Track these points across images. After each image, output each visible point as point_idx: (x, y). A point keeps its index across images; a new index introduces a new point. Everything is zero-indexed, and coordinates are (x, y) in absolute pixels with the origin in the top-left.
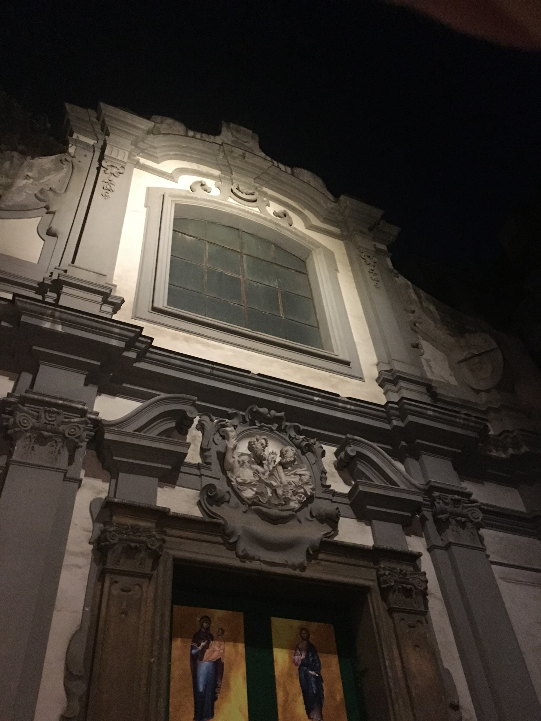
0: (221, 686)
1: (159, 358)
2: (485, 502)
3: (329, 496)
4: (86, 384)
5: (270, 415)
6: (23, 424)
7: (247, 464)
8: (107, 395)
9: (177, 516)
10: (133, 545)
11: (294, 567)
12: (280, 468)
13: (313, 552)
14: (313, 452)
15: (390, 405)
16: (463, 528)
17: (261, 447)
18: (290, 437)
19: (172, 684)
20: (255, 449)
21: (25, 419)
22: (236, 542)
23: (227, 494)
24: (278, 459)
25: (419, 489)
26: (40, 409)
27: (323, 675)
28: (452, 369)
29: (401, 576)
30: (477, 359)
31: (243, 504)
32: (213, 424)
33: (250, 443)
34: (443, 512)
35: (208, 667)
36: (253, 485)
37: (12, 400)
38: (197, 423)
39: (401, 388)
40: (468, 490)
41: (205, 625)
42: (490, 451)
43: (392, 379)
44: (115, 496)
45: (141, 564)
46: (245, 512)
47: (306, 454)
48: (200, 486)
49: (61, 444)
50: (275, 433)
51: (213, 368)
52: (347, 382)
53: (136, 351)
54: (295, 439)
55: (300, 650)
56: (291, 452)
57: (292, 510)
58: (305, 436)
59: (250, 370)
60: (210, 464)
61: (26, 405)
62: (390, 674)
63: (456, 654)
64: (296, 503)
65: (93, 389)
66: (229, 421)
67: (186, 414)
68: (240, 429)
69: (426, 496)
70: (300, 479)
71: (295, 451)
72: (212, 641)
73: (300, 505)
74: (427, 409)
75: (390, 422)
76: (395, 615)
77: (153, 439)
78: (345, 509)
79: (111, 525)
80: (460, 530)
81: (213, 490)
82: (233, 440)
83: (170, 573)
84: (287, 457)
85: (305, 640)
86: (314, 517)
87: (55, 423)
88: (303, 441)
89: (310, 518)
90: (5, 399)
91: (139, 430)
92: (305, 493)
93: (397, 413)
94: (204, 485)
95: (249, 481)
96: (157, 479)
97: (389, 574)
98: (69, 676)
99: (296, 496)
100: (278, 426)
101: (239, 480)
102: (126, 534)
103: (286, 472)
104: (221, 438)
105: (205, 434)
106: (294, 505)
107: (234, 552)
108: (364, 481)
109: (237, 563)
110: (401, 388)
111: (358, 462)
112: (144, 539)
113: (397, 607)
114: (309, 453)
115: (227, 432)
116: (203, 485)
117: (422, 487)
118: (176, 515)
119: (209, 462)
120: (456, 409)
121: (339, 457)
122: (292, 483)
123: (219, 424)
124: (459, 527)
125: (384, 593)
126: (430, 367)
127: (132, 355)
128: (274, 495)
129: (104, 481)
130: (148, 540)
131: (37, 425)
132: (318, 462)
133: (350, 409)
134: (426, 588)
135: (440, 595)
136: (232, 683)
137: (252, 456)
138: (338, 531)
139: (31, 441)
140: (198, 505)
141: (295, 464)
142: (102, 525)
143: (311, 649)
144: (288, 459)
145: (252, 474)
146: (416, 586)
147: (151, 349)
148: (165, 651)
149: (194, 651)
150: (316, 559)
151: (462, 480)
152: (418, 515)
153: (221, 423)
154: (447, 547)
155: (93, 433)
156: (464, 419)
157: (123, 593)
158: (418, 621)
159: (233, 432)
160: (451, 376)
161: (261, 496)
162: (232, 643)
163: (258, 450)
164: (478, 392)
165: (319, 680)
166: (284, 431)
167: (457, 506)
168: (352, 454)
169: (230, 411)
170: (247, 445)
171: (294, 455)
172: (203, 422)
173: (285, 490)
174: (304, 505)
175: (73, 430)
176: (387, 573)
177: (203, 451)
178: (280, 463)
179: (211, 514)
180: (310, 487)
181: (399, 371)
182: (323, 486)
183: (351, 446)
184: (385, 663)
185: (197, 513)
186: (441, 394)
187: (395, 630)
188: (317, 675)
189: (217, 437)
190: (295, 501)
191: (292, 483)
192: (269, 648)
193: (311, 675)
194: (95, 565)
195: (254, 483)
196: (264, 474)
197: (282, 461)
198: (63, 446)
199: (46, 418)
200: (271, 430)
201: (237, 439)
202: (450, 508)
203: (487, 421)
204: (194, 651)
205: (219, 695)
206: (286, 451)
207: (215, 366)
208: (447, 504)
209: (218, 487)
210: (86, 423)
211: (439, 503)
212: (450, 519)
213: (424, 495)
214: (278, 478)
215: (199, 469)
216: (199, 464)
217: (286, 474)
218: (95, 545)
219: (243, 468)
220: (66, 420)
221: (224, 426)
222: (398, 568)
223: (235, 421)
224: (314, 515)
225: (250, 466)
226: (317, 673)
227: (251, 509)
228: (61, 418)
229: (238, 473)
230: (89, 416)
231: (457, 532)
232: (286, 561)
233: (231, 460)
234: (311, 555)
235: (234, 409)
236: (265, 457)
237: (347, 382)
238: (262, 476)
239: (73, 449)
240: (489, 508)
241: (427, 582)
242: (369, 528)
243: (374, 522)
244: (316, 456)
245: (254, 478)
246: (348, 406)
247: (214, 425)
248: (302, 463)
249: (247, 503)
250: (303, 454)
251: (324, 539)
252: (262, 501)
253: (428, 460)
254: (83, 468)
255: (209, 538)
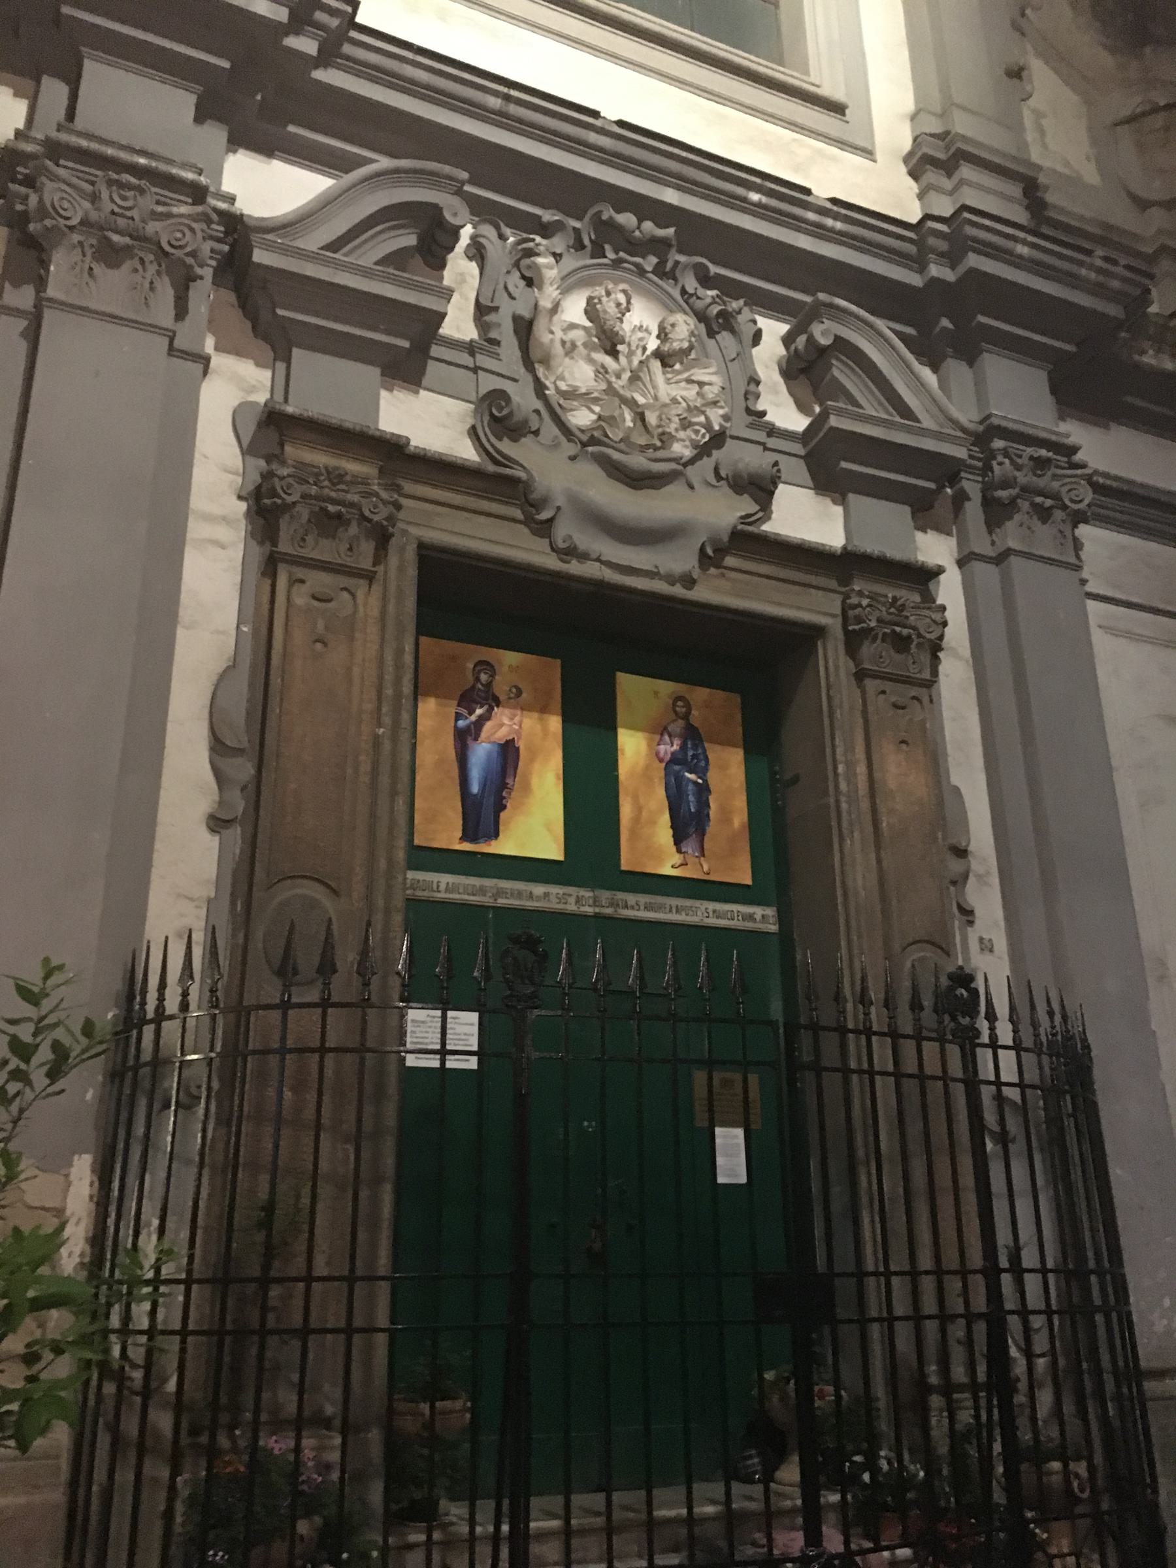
0: (513, 785)
1: (373, 58)
2: (1102, 468)
3: (760, 436)
4: (199, 119)
5: (640, 232)
6: (62, 212)
7: (581, 349)
8: (253, 154)
9: (425, 455)
10: (332, 508)
11: (671, 579)
12: (656, 365)
13: (715, 551)
14: (733, 331)
15: (931, 224)
16: (1044, 522)
17: (616, 310)
18: (684, 292)
19: (418, 778)
20: (602, 315)
21: (66, 199)
22: (551, 521)
23: (534, 417)
24: (653, 344)
25: (964, 430)
26: (96, 176)
27: (710, 782)
28: (1094, 141)
29: (892, 610)
30: (1159, 120)
31: (569, 441)
32: (504, 247)
33: (590, 300)
34: (1006, 484)
35: (489, 755)
36: (593, 398)
37: (29, 148)
38: (468, 241)
39: (962, 182)
40: (1071, 440)
41: (484, 677)
42: (1143, 352)
43: (941, 156)
44: (286, 400)
45: (350, 549)
46: (573, 458)
47: (718, 337)
48: (474, 394)
49: (154, 267)
50: (649, 280)
51: (507, 98)
52: (833, 159)
53: (319, 35)
54: (695, 298)
55: (670, 736)
56: (684, 326)
57: (676, 460)
58: (718, 292)
59: (598, 109)
60: (498, 343)
61: (62, 162)
62: (843, 786)
63: (979, 761)
64: (686, 447)
65: (216, 134)
66: (544, 242)
67: (444, 217)
68: (571, 262)
69: (976, 449)
70: (698, 393)
71: (692, 327)
72: (498, 706)
73: (695, 452)
74: (1015, 239)
75: (922, 269)
76: (871, 685)
77: (365, 273)
78: (794, 467)
79: (283, 463)
80: (1036, 524)
81: (503, 404)
82: (551, 289)
83: (412, 572)
84: (674, 341)
85: (682, 719)
86: (722, 479)
87: (134, 213)
88: (714, 302)
89: (714, 482)
90: (11, 145)
91: (335, 246)
92: (708, 426)
93: (943, 246)
94: (485, 392)
95: (583, 390)
96: (378, 371)
97: (869, 605)
98: (219, 747)
99: (688, 430)
100: (658, 263)
101: (563, 386)
102: (316, 485)
103: (669, 376)
104: (522, 283)
105: (488, 267)
106: (680, 449)
107: (547, 540)
108: (841, 405)
109: (551, 562)
110: (962, 182)
111: (834, 362)
112: (356, 498)
113: (877, 668)
114: (725, 334)
115: (536, 267)
116: (483, 391)
117: (971, 426)
118: (422, 453)
119: (495, 339)
120: (1087, 245)
121: (793, 348)
122: (680, 400)
123: (520, 247)
124: (1035, 518)
125: (853, 642)
126: (1042, 132)
127: (306, 45)
128: (639, 423)
129: (258, 365)
130: (364, 501)
131: (94, 216)
132: (743, 357)
133: (832, 230)
134: (941, 637)
135: (966, 652)
136: (535, 781)
137: (594, 332)
138: (771, 512)
139: (84, 255)
140: (469, 434)
141: (690, 357)
142: (262, 463)
143: (692, 735)
144: (676, 345)
145: (592, 375)
146: (922, 632)
147: (354, 34)
148: (405, 717)
149: (461, 723)
150: (718, 566)
151: (1062, 417)
152: (951, 488)
153: (524, 246)
154: (1000, 559)
155: (226, 248)
156: (1099, 271)
157: (316, 603)
158: (914, 698)
159: (552, 268)
160: (1088, 159)
161: (611, 426)
162: (536, 715)
163: (607, 317)
164: (1143, 204)
165: (703, 790)
166: (672, 276)
167: (1039, 472)
168: (824, 341)
169: (548, 216)
170: (583, 304)
171: (690, 336)
172: (482, 240)
173: (664, 417)
174: (703, 451)
175: (179, 235)
176: (865, 602)
177: (482, 311)
178: (658, 354)
179: (499, 458)
180: (721, 412)
181: (964, 138)
182: (749, 411)
183: (823, 322)
184: (835, 768)
185: (467, 452)
186: (1055, 207)
187: (865, 712)
188: (700, 781)
189: (515, 282)
190: (683, 440)
191: (680, 400)
192: (612, 728)
193: (688, 779)
194: (253, 543)
195: (595, 395)
196: (618, 376)
197: (662, 349)
198: (159, 273)
199: (112, 201)
200: (641, 272)
201: (563, 287)
202: (1023, 478)
203: (1151, 277)
204: (461, 723)
205: (510, 801)
206: (673, 325)
207: (514, 93)
208: (1018, 468)
209: (516, 398)
210: (206, 219)
211: (1000, 464)
212: (1019, 501)
213: (971, 445)
214: (650, 387)
215: (472, 354)
216: (472, 341)
217: (669, 379)
218: (251, 502)
219: (572, 358)
220: (160, 209)
221: (530, 253)
222: (890, 595)
223: (559, 243)
224: (723, 475)
225: (589, 355)
226: (700, 778)
227: (587, 452)
228: (147, 203)
229: (561, 369)
230: (213, 202)
231: (1029, 528)
232: (656, 567)
233: (546, 338)
234: (710, 558)
235: (555, 212)
236: (622, 336)
237: (833, 159)
238: (613, 379)
239: (184, 283)
240: (1108, 482)
241: (945, 624)
242: (839, 510)
243: (851, 497)
244: (741, 342)
245: (596, 384)
246: (830, 222)
247: (507, 251)
248: (707, 357)
249: (577, 438)
250: (711, 334)
251: (740, 527)
252: (610, 435)
253: (995, 365)
254: (209, 330)
255: (495, 507)
